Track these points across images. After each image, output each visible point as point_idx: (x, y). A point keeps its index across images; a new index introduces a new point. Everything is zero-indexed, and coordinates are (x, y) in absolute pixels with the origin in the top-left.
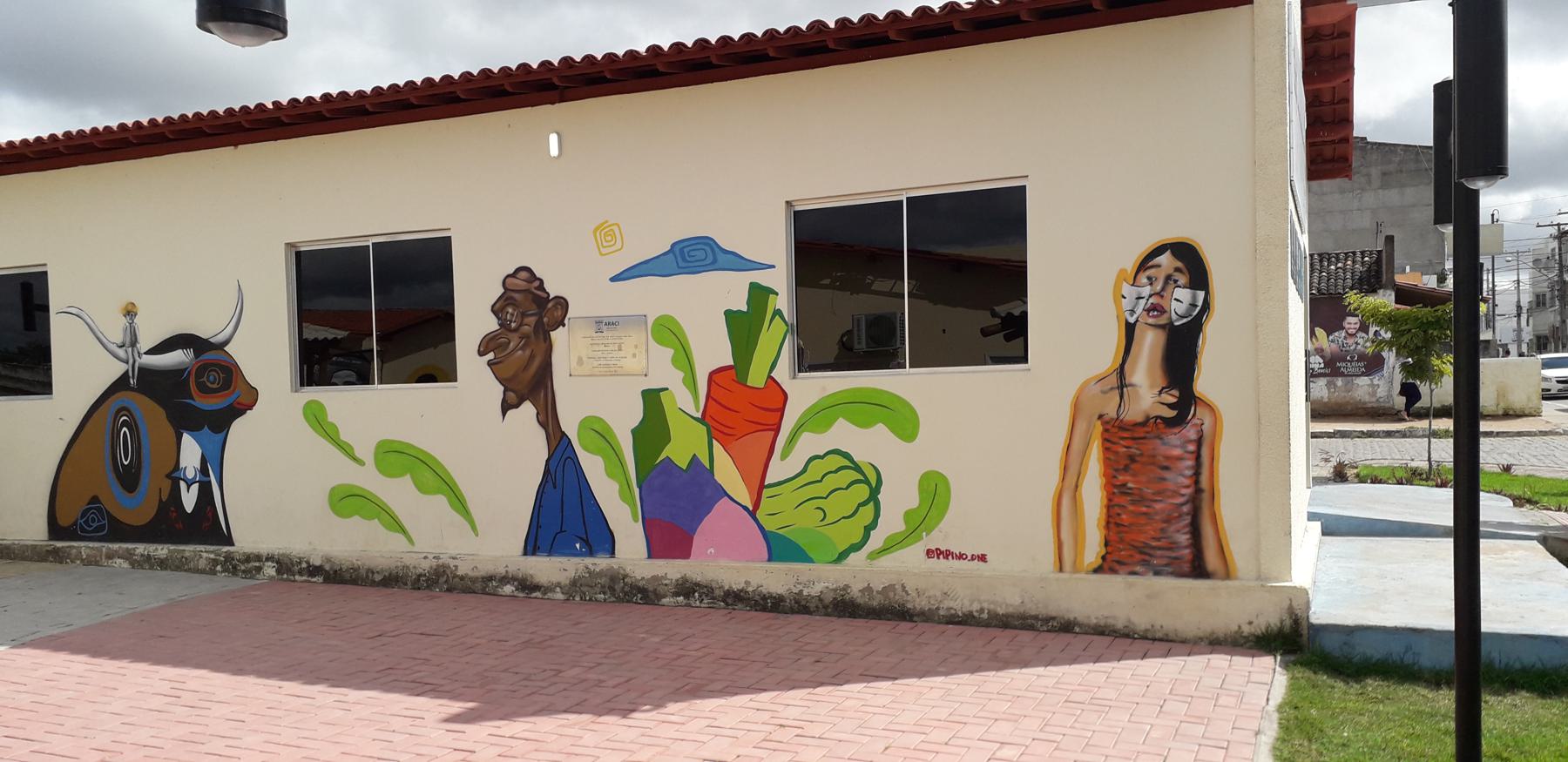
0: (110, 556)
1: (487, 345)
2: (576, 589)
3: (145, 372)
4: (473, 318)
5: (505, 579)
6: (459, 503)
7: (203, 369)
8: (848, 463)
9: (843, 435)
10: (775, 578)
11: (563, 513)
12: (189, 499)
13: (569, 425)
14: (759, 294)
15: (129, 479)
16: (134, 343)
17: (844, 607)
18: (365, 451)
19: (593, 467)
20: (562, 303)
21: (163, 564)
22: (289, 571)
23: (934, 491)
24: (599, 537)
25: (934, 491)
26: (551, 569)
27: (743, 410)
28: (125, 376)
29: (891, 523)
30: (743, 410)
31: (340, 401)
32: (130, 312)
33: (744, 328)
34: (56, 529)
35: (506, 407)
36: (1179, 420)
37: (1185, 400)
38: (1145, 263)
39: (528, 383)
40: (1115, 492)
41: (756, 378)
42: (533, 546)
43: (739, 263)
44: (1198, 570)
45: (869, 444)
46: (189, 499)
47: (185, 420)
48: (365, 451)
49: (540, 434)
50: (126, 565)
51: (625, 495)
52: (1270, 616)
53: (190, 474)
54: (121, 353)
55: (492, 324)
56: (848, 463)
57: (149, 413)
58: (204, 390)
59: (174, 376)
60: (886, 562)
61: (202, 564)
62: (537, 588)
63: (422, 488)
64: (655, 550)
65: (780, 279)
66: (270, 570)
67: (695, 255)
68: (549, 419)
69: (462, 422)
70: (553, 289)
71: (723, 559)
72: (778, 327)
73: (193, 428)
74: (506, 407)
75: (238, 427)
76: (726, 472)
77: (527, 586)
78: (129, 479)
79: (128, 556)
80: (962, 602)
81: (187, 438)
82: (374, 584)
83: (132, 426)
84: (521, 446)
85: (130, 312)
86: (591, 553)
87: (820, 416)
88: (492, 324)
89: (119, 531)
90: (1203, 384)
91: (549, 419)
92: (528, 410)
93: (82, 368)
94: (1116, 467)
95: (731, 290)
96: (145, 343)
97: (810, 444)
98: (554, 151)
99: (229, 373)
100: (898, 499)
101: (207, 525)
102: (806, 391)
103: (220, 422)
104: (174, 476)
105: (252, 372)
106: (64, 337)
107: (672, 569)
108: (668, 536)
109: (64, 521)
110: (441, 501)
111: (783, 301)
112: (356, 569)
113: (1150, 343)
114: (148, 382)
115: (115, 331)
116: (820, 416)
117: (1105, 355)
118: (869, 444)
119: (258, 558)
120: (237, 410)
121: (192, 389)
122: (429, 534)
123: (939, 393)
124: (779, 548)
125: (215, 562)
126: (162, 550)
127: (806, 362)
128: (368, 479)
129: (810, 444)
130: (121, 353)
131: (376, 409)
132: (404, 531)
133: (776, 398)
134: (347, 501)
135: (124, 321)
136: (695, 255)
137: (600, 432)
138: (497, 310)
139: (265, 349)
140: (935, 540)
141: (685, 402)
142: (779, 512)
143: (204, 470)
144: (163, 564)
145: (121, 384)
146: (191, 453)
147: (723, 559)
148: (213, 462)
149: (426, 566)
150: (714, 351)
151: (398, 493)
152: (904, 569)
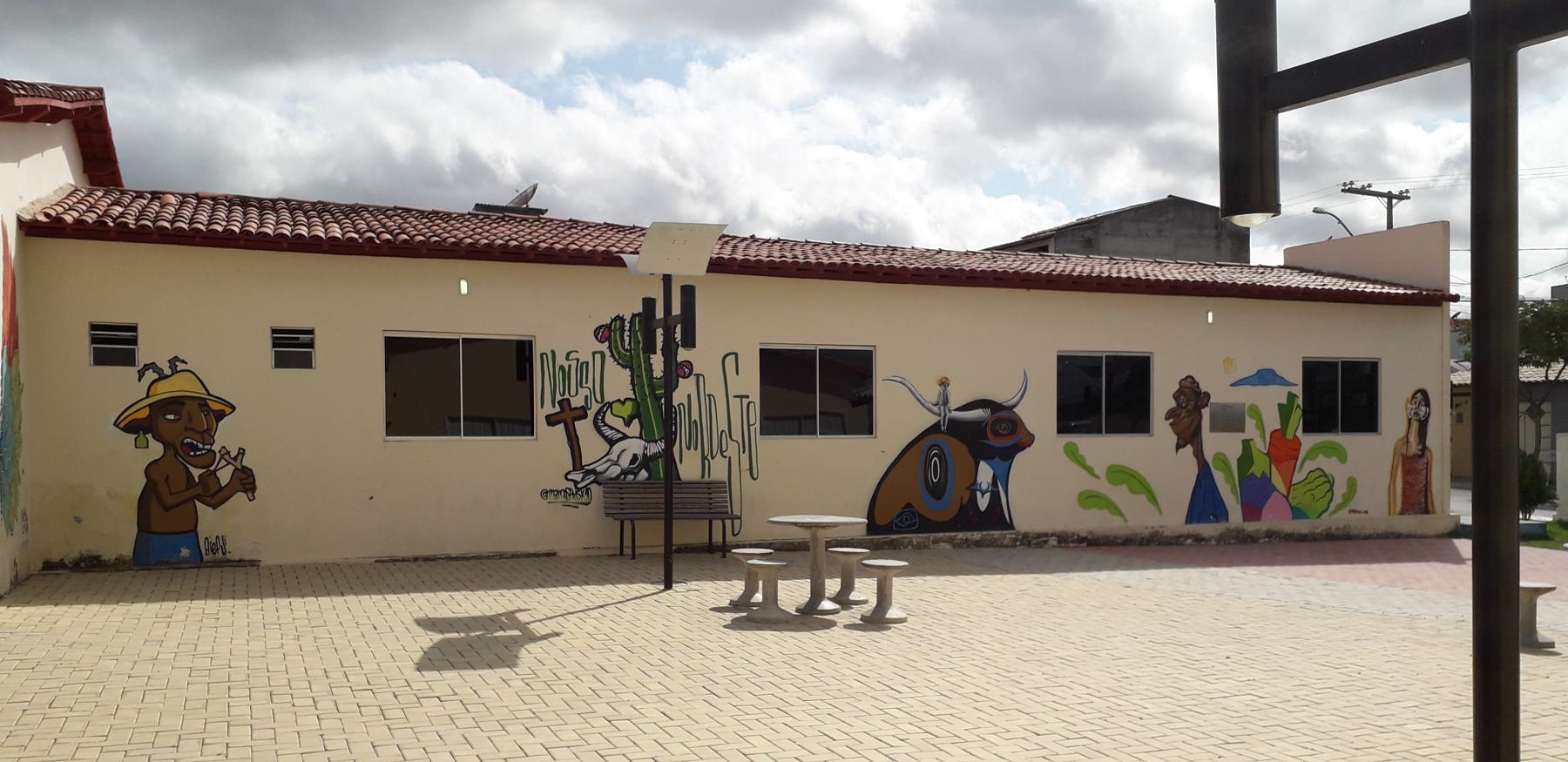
0: (935, 542)
1: (1170, 414)
2: (1222, 539)
3: (952, 421)
4: (1162, 398)
5: (1188, 537)
6: (1153, 499)
7: (998, 421)
8: (154, 504)
9: (1322, 462)
10: (1301, 526)
11: (1205, 502)
12: (983, 502)
13: (1209, 457)
14: (1291, 396)
15: (937, 492)
16: (946, 402)
17: (1330, 537)
18: (1101, 471)
19: (1219, 477)
20: (1207, 395)
21: (978, 544)
22: (1066, 541)
23: (1352, 484)
24: (1220, 513)
25: (1352, 484)
26: (1208, 529)
27: (1283, 451)
28: (937, 425)
29: (1337, 500)
30: (1283, 451)
31: (1088, 444)
32: (944, 383)
33: (1285, 411)
34: (872, 527)
35: (1178, 447)
36: (1422, 456)
37: (1424, 448)
38: (1414, 396)
39: (1189, 435)
40: (1405, 482)
41: (1289, 436)
42: (1190, 519)
43: (1284, 382)
44: (1426, 512)
45: (1330, 465)
46: (983, 502)
47: (981, 452)
48: (1101, 471)
49: (1195, 462)
50: (948, 547)
51: (1233, 492)
52: (1449, 526)
53: (984, 487)
54: (935, 409)
55: (1173, 404)
56: (154, 504)
57: (956, 450)
58: (997, 434)
59: (976, 425)
60: (1336, 516)
61: (1006, 542)
62: (1203, 539)
63: (1133, 491)
64: (1246, 518)
65: (1298, 391)
66: (1053, 541)
67: (1266, 377)
68: (1199, 454)
69: (1156, 454)
70: (1203, 388)
71: (1274, 519)
72: (1299, 412)
73: (987, 459)
74: (1178, 447)
75: (1020, 459)
76: (1277, 480)
77: (1198, 539)
78: (937, 492)
79: (950, 541)
80: (1369, 530)
81: (982, 464)
82: (1117, 544)
83: (942, 457)
84: (1185, 467)
85: (944, 383)
86: (1217, 521)
87: (1312, 454)
88: (1173, 404)
89: (927, 526)
90: (1428, 443)
91: (1199, 454)
92: (1189, 449)
93: (900, 416)
94: (1406, 473)
95: (1278, 394)
96: (954, 404)
97: (1310, 465)
98: (1210, 320)
99: (1015, 424)
100: (1340, 489)
101: (996, 518)
102: (1308, 441)
103: (1008, 455)
104: (973, 488)
105: (1030, 423)
106: (883, 393)
107: (1251, 527)
108: (1252, 510)
109: (881, 520)
110: (1143, 497)
111: (1300, 401)
112: (1107, 537)
113: (1415, 425)
114: (956, 429)
115: (932, 394)
116: (1312, 454)
117: (1402, 433)
118: (1330, 465)
119: (1046, 535)
120: (1021, 447)
121: (991, 434)
122: (1138, 516)
123: (1353, 443)
124: (1297, 513)
125: (1016, 540)
126: (977, 535)
127: (1308, 429)
128: (1103, 487)
129: (1310, 465)
130: (935, 409)
131: (1105, 448)
132: (1121, 514)
133: (1297, 444)
134: (1089, 499)
135: (939, 389)
136: (1266, 377)
137: (1222, 459)
138: (1176, 396)
139: (1039, 411)
140: (1352, 506)
141: (1260, 446)
142: (1298, 497)
143: (994, 484)
144: (978, 544)
145: (934, 429)
146: (985, 473)
147: (1274, 519)
148: (1001, 478)
149: (1147, 532)
150: (1273, 422)
151: (1120, 494)
152: (1337, 519)
